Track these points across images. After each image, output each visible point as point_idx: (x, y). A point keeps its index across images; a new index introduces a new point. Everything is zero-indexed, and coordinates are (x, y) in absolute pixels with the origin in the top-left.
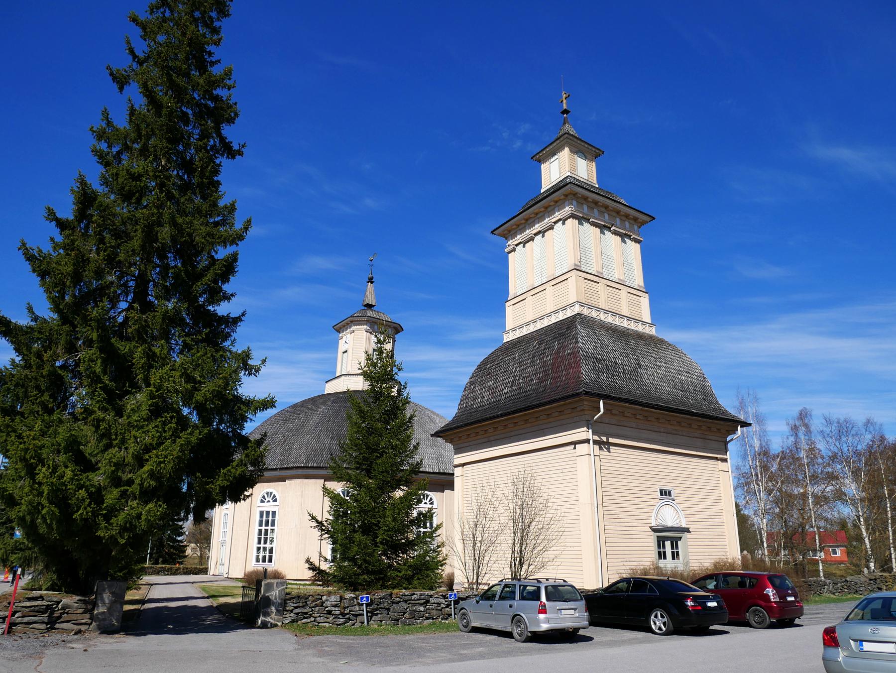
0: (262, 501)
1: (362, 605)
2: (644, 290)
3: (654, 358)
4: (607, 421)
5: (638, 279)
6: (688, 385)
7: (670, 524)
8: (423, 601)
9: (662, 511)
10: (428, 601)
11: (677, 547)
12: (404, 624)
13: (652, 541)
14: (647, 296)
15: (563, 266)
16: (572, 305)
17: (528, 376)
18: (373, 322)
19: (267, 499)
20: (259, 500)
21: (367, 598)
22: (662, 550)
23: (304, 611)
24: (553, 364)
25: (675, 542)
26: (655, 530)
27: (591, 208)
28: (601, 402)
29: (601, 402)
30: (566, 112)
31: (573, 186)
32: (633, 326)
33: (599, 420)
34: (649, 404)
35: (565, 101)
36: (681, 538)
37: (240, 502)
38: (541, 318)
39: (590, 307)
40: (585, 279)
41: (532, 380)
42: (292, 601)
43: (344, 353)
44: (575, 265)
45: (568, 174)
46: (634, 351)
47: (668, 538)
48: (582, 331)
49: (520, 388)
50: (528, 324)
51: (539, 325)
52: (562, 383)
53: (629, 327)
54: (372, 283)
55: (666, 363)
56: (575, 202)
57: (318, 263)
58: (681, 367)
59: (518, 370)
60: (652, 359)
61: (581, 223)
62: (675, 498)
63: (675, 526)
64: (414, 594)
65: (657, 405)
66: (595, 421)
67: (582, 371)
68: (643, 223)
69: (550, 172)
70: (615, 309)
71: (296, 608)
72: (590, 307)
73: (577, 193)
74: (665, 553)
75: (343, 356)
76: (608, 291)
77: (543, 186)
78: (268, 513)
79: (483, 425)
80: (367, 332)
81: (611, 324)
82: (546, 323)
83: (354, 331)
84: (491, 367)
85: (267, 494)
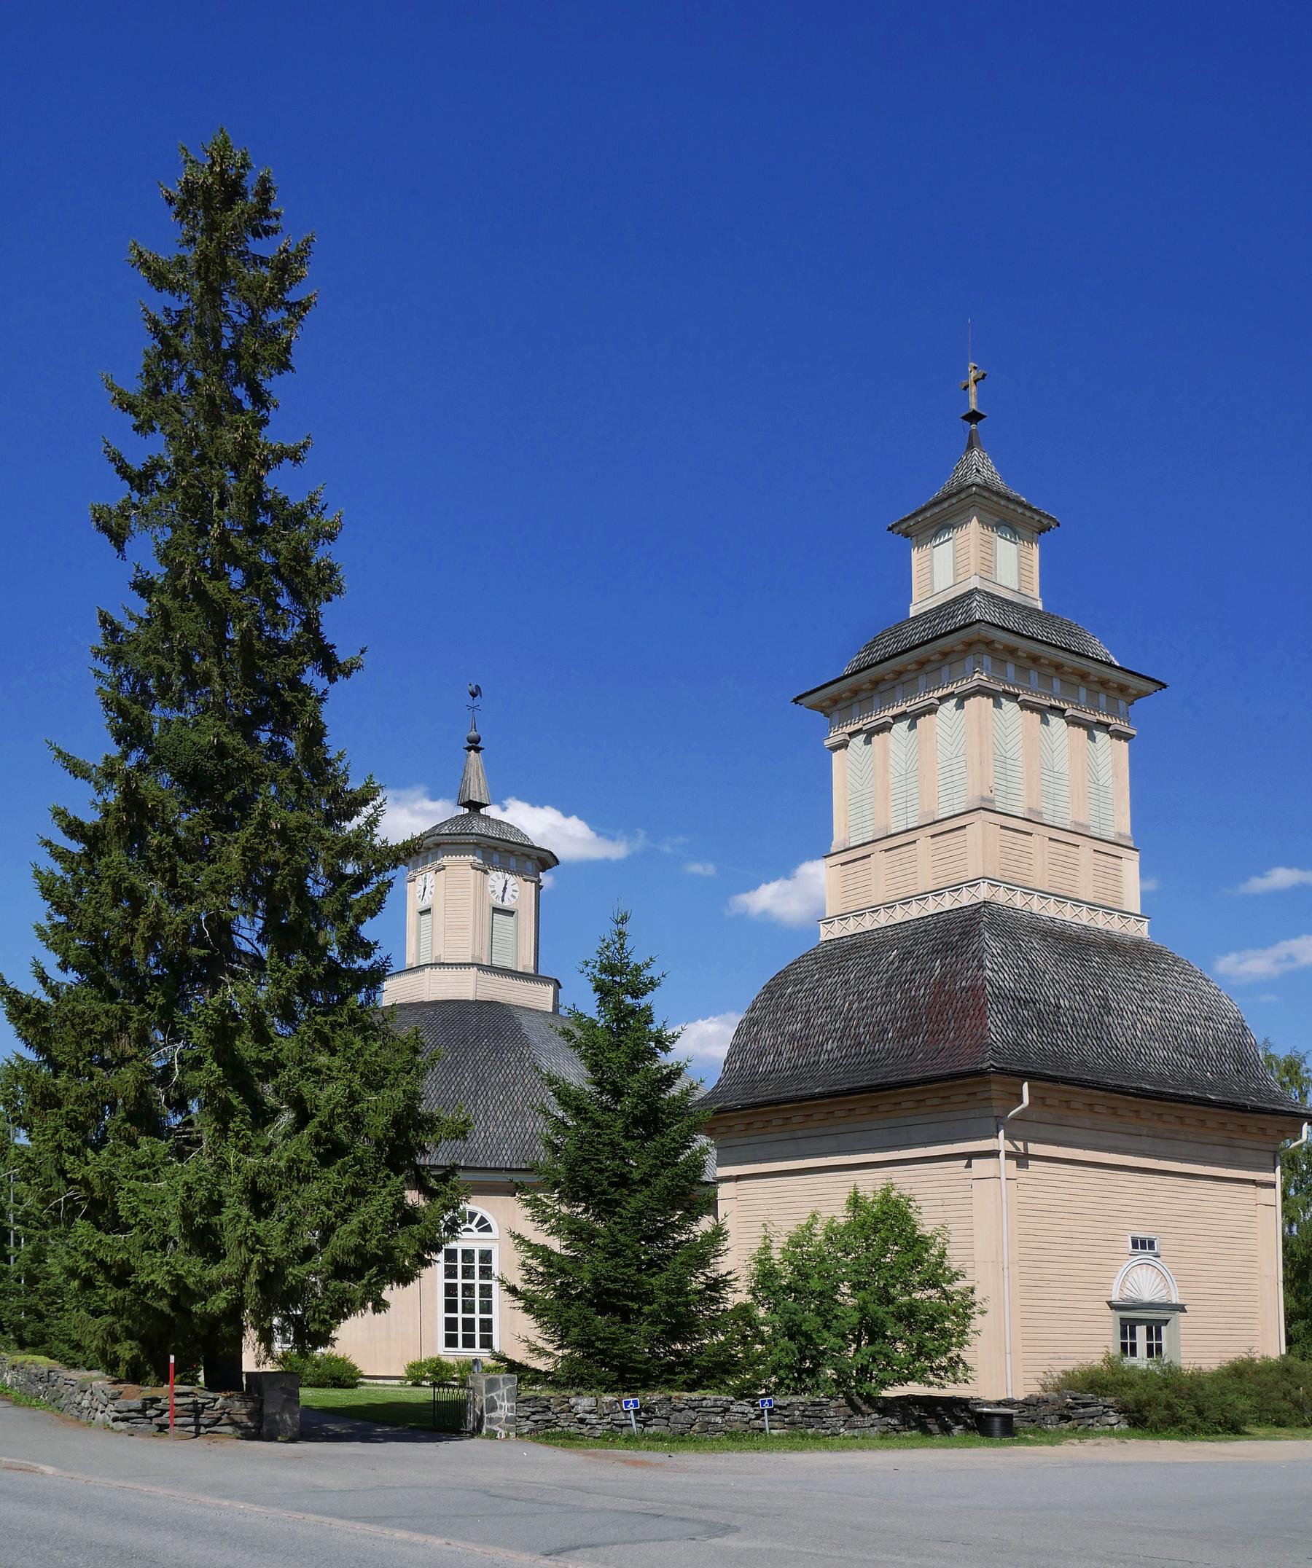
1: (629, 1411)
2: (1131, 844)
3: (1140, 992)
4: (1034, 1118)
5: (1120, 822)
6: (1207, 1044)
7: (1147, 1297)
8: (719, 1409)
9: (1134, 1275)
10: (727, 1410)
11: (1159, 1336)
12: (692, 1440)
13: (1111, 1325)
14: (1136, 856)
15: (955, 796)
16: (973, 883)
17: (878, 1023)
18: (489, 847)
21: (635, 1402)
22: (1129, 1341)
23: (547, 1418)
24: (929, 1007)
25: (1154, 1329)
26: (1113, 1306)
27: (1022, 670)
30: (974, 417)
31: (986, 628)
32: (1100, 922)
33: (1020, 1117)
34: (1120, 1086)
35: (973, 389)
36: (1167, 1321)
38: (906, 901)
39: (1011, 886)
40: (1002, 827)
41: (886, 1031)
42: (527, 1404)
43: (422, 913)
44: (983, 799)
45: (974, 583)
46: (1099, 979)
47: (1141, 1321)
48: (992, 944)
49: (860, 1044)
50: (875, 910)
51: (899, 915)
52: (947, 1045)
53: (1092, 924)
54: (478, 750)
55: (1163, 1002)
56: (987, 660)
58: (1195, 1008)
59: (854, 1007)
60: (1136, 994)
61: (998, 705)
62: (1162, 1253)
63: (1158, 1300)
64: (705, 1399)
65: (1136, 1089)
66: (1013, 1119)
67: (990, 1025)
69: (931, 566)
70: (1064, 887)
71: (533, 1413)
72: (1011, 886)
73: (993, 642)
74: (1134, 1346)
75: (419, 921)
76: (1051, 850)
77: (915, 598)
79: (783, 1109)
80: (478, 869)
81: (1052, 920)
82: (914, 911)
83: (444, 868)
84: (794, 993)
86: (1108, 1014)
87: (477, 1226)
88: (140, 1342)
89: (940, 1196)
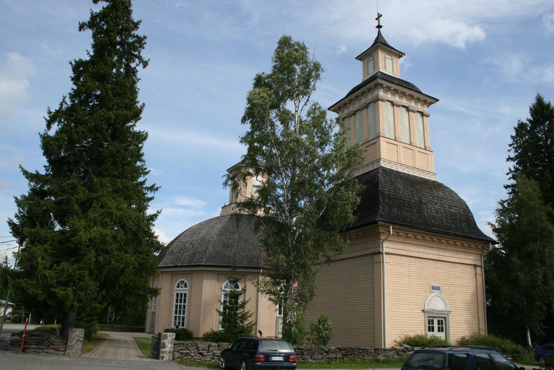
0: (178, 287)
19: (181, 286)
20: (176, 286)
28: (391, 226)
29: (391, 226)
37: (147, 209)
57: (185, 202)
62: (443, 292)
68: (431, 103)
71: (181, 350)
78: (181, 294)
85: (181, 282)
86: (422, 204)
87: (184, 285)
88: (445, 341)
89: (364, 270)
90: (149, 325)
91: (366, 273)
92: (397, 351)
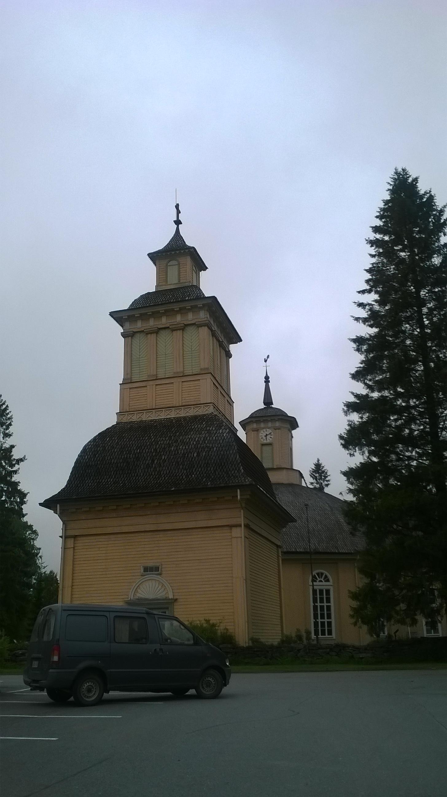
78: (321, 591)
90: (132, 616)
91: (140, 367)
92: (115, 641)
